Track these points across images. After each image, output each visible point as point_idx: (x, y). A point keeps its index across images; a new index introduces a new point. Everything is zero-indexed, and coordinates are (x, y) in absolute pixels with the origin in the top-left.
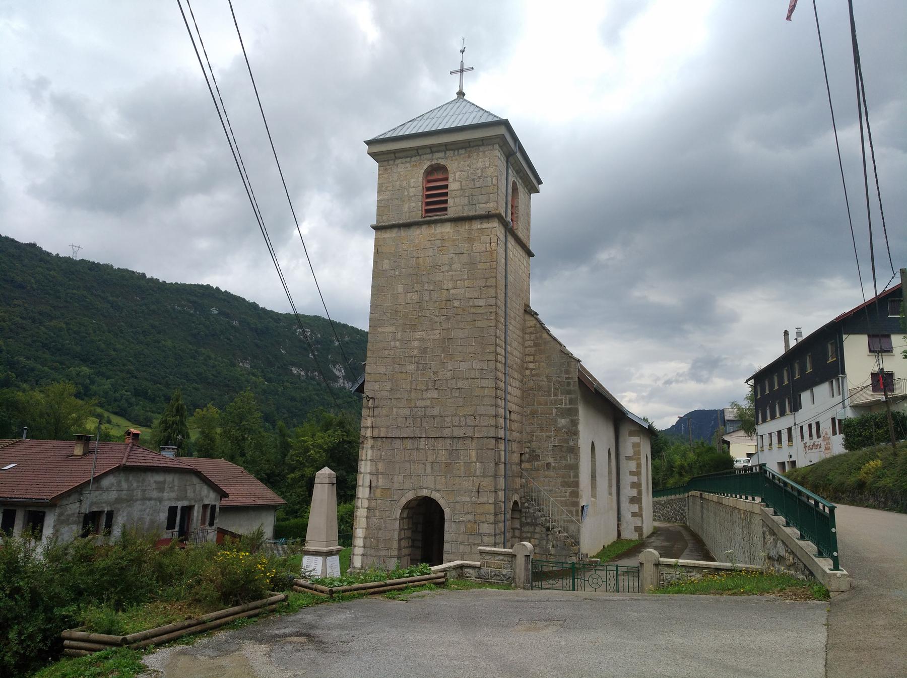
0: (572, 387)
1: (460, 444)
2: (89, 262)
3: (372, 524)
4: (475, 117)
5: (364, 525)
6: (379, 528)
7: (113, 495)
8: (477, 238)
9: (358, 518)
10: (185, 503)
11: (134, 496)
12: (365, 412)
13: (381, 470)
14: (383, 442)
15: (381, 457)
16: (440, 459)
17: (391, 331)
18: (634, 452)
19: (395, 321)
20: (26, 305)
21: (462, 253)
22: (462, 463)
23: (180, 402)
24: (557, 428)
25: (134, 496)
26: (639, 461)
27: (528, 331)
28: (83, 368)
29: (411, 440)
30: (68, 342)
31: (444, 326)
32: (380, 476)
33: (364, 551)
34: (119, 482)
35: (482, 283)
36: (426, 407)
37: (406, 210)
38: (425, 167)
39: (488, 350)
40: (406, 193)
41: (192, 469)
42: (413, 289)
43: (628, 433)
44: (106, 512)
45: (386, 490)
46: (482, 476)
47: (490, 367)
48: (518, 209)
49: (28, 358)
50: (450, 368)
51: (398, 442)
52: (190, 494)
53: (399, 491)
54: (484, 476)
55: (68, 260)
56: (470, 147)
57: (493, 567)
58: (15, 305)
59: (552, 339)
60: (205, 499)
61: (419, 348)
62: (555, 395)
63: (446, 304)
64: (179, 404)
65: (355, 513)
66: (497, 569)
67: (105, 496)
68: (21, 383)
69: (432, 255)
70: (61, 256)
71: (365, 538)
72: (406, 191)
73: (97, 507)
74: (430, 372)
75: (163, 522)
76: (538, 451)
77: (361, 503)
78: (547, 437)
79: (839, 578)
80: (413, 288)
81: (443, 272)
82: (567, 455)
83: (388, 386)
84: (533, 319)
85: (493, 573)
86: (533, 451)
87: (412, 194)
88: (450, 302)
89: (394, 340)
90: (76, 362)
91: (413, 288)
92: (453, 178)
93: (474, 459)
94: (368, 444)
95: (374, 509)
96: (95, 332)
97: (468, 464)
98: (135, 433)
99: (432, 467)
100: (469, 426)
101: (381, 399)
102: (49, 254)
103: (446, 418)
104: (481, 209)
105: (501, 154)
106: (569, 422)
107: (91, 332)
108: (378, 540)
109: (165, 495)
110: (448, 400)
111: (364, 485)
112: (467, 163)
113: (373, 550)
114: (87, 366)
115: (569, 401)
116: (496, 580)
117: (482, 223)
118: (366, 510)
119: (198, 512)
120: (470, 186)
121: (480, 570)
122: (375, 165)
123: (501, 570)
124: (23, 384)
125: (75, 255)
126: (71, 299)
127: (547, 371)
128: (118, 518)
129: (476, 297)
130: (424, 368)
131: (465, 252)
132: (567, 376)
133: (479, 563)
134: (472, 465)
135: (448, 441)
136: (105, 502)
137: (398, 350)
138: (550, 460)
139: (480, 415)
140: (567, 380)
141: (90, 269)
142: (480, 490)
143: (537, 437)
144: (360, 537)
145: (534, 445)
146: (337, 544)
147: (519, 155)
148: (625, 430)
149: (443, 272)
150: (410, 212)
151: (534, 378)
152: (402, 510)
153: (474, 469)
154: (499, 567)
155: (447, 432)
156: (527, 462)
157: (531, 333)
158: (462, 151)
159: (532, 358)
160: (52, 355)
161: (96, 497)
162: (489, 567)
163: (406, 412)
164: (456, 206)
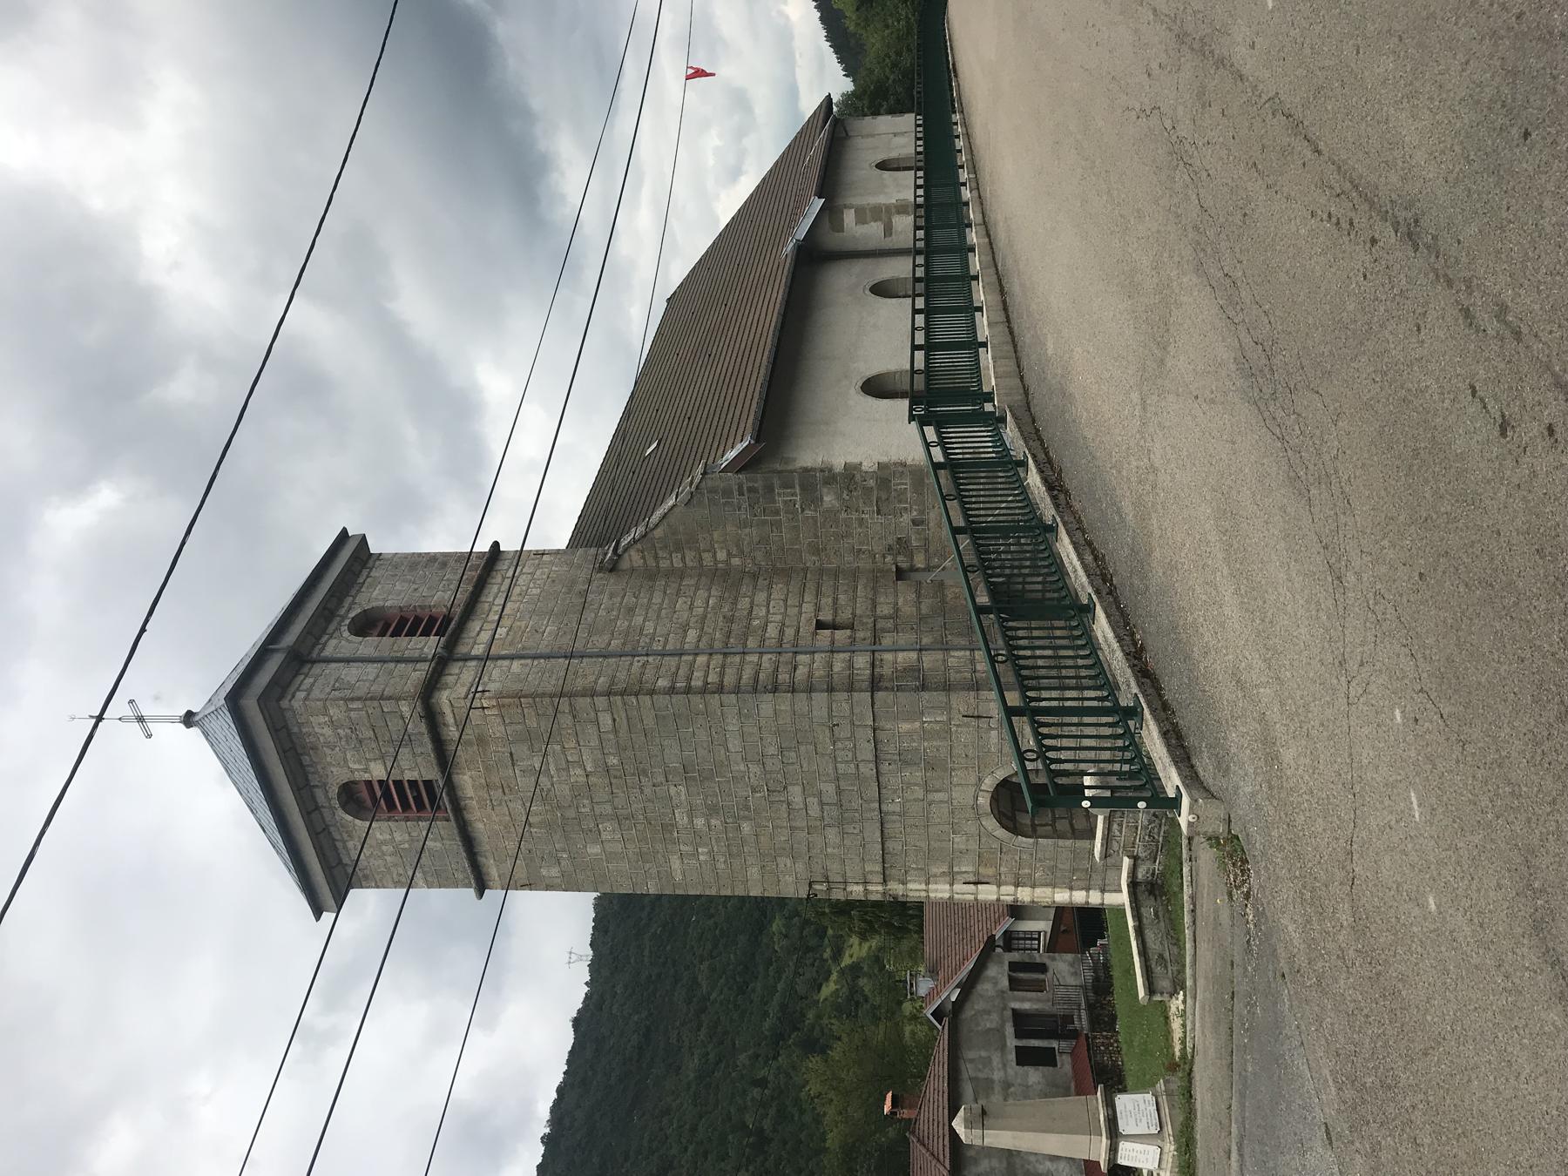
0: (759, 485)
1: (890, 750)
2: (593, 935)
3: (1045, 879)
5: (1048, 890)
6: (1053, 869)
8: (476, 731)
9: (1035, 900)
10: (1009, 1030)
12: (838, 895)
13: (945, 869)
14: (891, 866)
15: (922, 869)
16: (920, 779)
17: (678, 862)
18: (875, 221)
19: (659, 856)
20: (678, 1024)
21: (511, 754)
22: (926, 744)
23: (827, 910)
24: (842, 509)
26: (893, 210)
27: (651, 562)
28: (774, 929)
29: (886, 825)
30: (732, 956)
31: (661, 779)
32: (956, 869)
33: (1095, 889)
35: (565, 720)
36: (822, 804)
37: (438, 845)
38: (350, 818)
39: (701, 706)
40: (407, 846)
41: (949, 1022)
42: (594, 830)
43: (837, 234)
45: (981, 860)
46: (949, 713)
47: (735, 702)
48: (405, 606)
49: (766, 1014)
50: (742, 767)
51: (890, 845)
52: (991, 1022)
53: (983, 840)
54: (948, 708)
55: (594, 967)
56: (294, 748)
57: (1135, 838)
58: (678, 1041)
59: (665, 522)
60: (999, 987)
61: (708, 817)
62: (777, 513)
63: (615, 777)
64: (831, 912)
65: (1026, 904)
66: (1139, 833)
68: (808, 1021)
69: (521, 802)
70: (589, 978)
71: (1071, 889)
72: (402, 846)
74: (753, 798)
75: (1044, 1076)
76: (891, 540)
77: (1008, 895)
78: (860, 526)
79: (1198, 817)
80: (591, 831)
81: (552, 785)
82: (895, 490)
83: (785, 862)
84: (626, 555)
85: (1147, 838)
86: (890, 548)
87: (406, 837)
88: (611, 772)
89: (696, 854)
90: (765, 941)
91: (591, 831)
92: (361, 773)
93: (917, 724)
94: (896, 888)
95: (1017, 876)
96: (712, 916)
97: (926, 735)
98: (892, 1105)
99: (936, 791)
100: (853, 733)
101: (811, 872)
102: (588, 997)
103: (840, 772)
104: (419, 728)
105: (298, 689)
106: (829, 489)
107: (712, 921)
108: (1074, 871)
109: (997, 1076)
110: (805, 769)
111: (975, 892)
112: (328, 751)
113: (1093, 875)
114: (770, 922)
115: (787, 488)
116: (1159, 833)
117: (444, 724)
118: (1019, 888)
119: (1023, 1000)
120: (374, 745)
121: (1139, 857)
122: (354, 895)
123: (1139, 828)
124: (809, 1019)
125: (585, 958)
126: (660, 958)
127: (729, 528)
129: (595, 728)
130: (747, 808)
131: (506, 749)
132: (736, 493)
133: (1126, 862)
134: (929, 728)
135: (885, 767)
137: (715, 849)
138: (906, 519)
139: (830, 716)
140: (745, 493)
141: (606, 932)
142: (976, 714)
143: (861, 543)
144: (1071, 896)
145: (878, 548)
146: (1093, 1097)
147: (290, 638)
148: (832, 240)
149: (552, 785)
150: (442, 839)
151: (746, 550)
152: (1017, 835)
153: (934, 726)
154: (1134, 830)
155: (868, 770)
156: (912, 559)
157: (656, 557)
158: (306, 760)
159: (705, 555)
160: (757, 978)
162: (1133, 844)
163: (832, 834)
164: (417, 766)
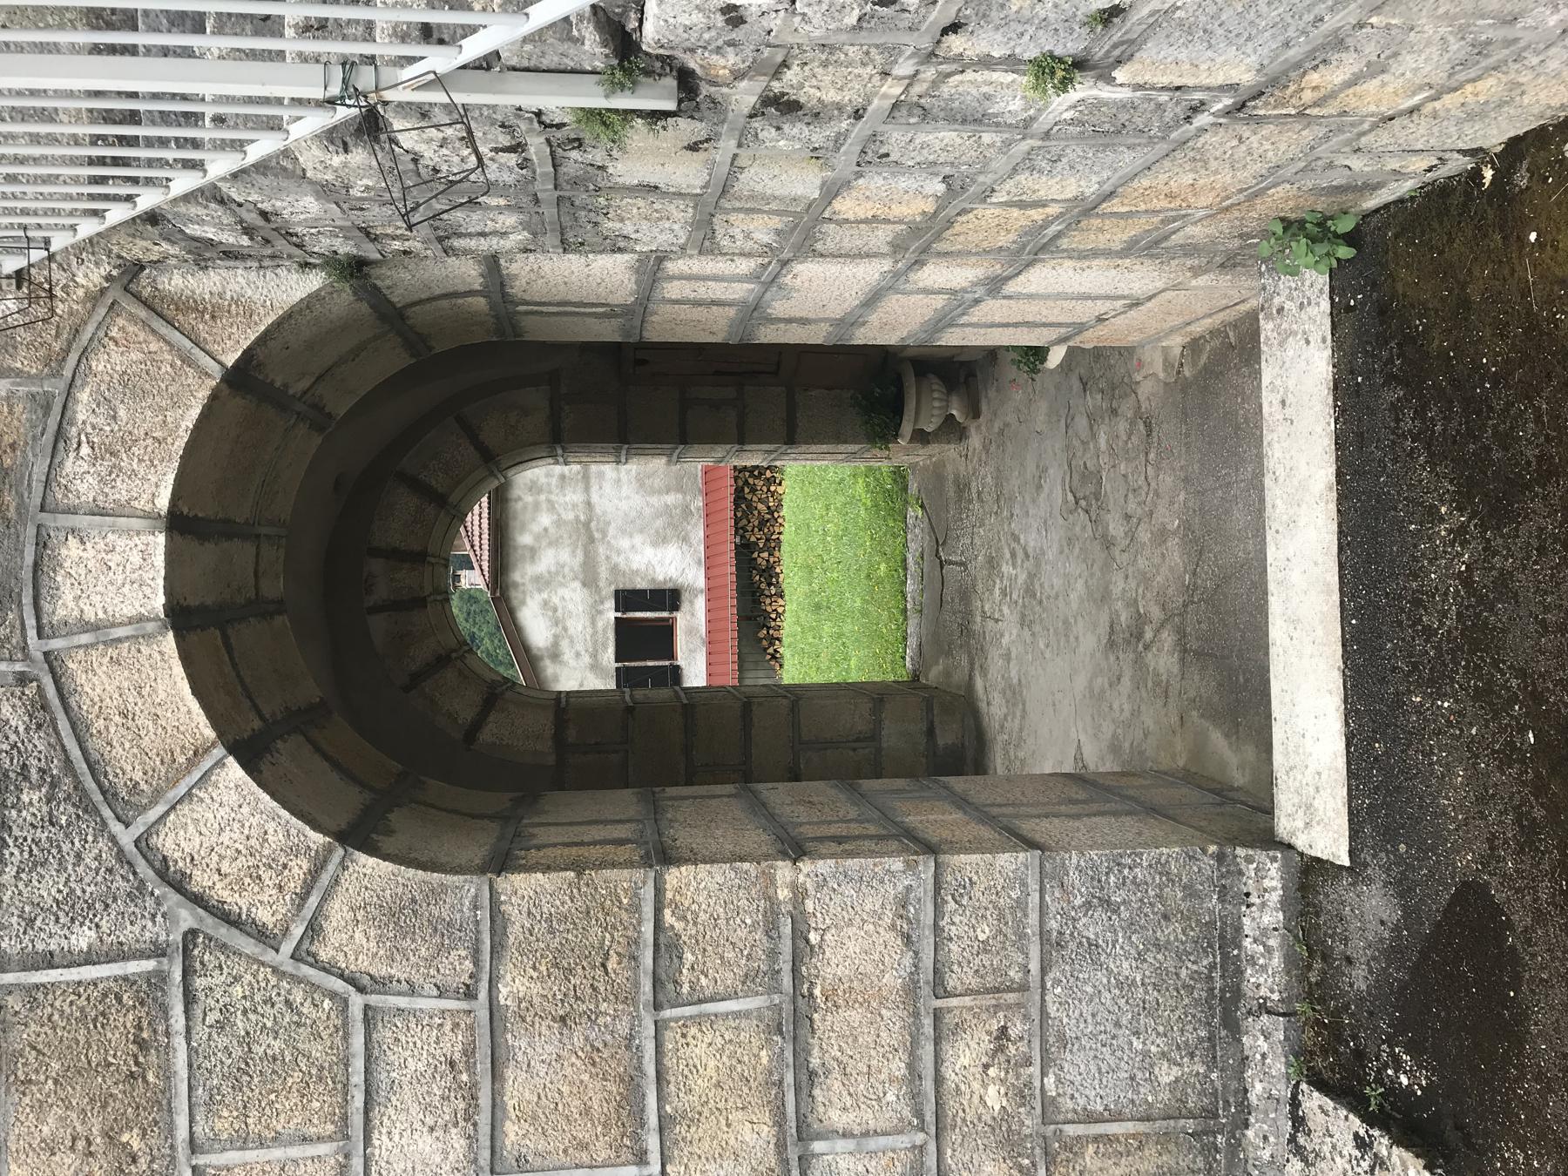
4: (1154, 296)
7: (573, 597)
11: (577, 517)
25: (577, 517)
34: (542, 582)
44: (619, 615)
67: (578, 626)
73: (605, 647)
128: (635, 566)
136: (593, 623)
161: (578, 655)
